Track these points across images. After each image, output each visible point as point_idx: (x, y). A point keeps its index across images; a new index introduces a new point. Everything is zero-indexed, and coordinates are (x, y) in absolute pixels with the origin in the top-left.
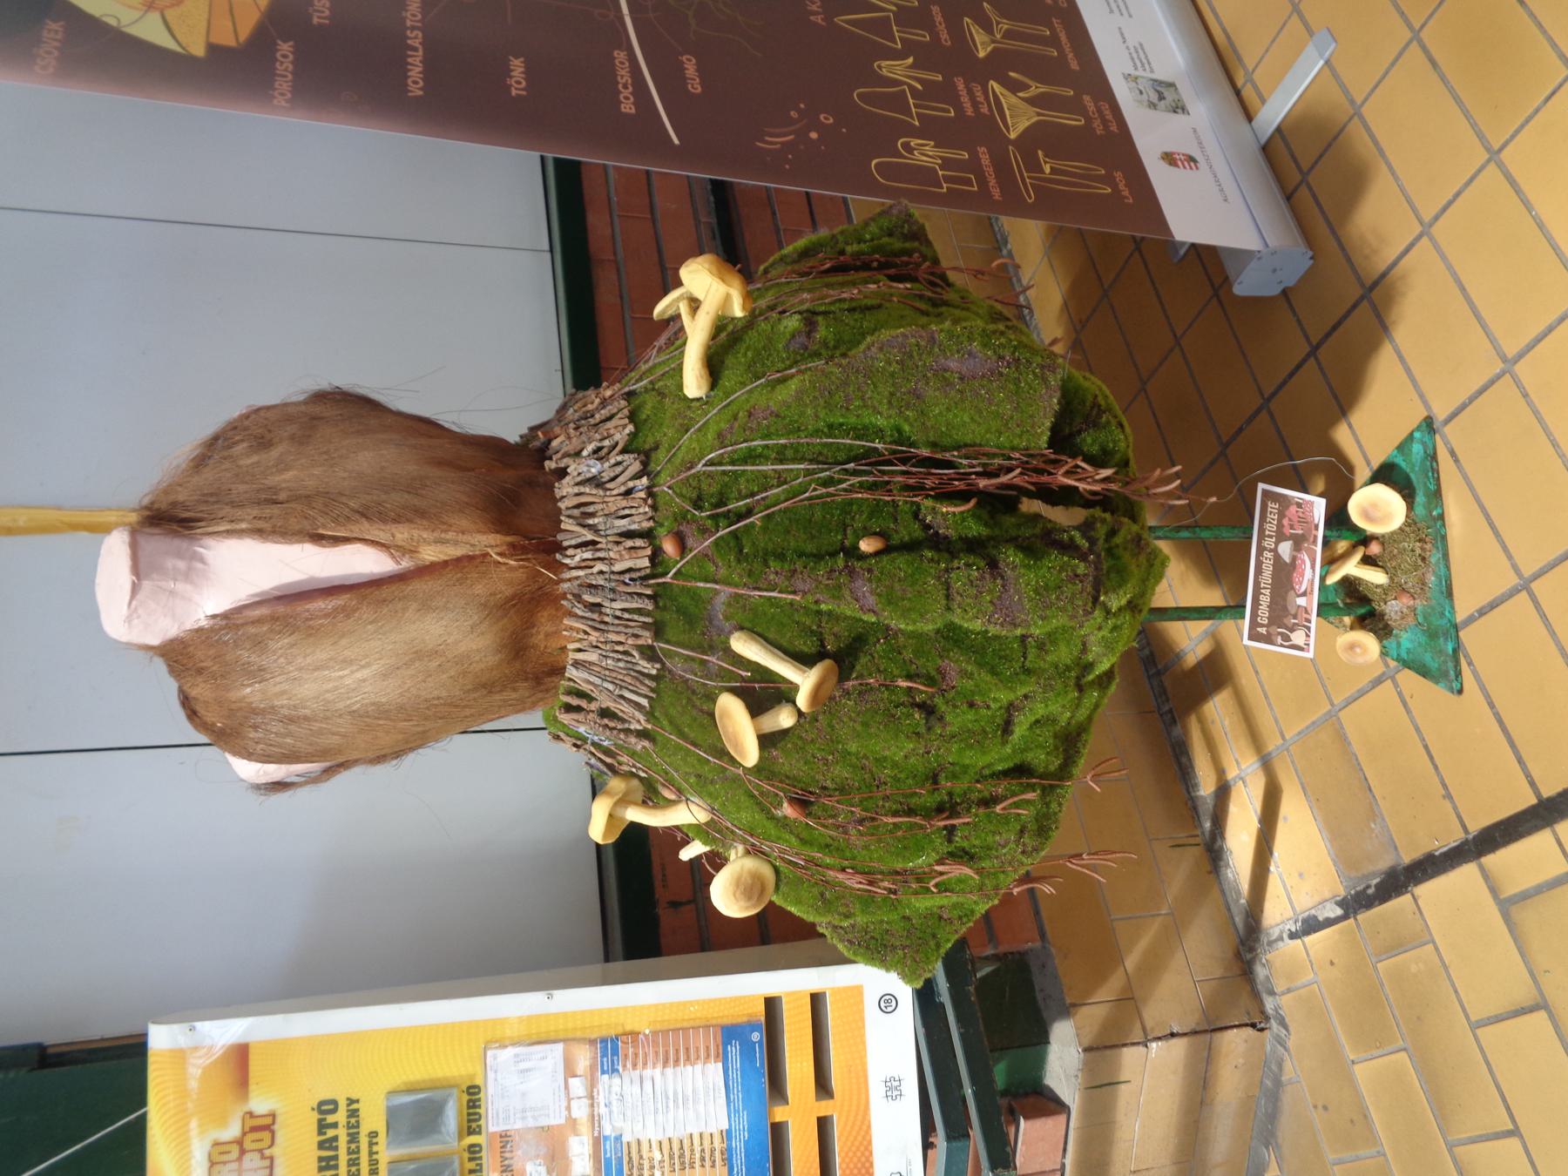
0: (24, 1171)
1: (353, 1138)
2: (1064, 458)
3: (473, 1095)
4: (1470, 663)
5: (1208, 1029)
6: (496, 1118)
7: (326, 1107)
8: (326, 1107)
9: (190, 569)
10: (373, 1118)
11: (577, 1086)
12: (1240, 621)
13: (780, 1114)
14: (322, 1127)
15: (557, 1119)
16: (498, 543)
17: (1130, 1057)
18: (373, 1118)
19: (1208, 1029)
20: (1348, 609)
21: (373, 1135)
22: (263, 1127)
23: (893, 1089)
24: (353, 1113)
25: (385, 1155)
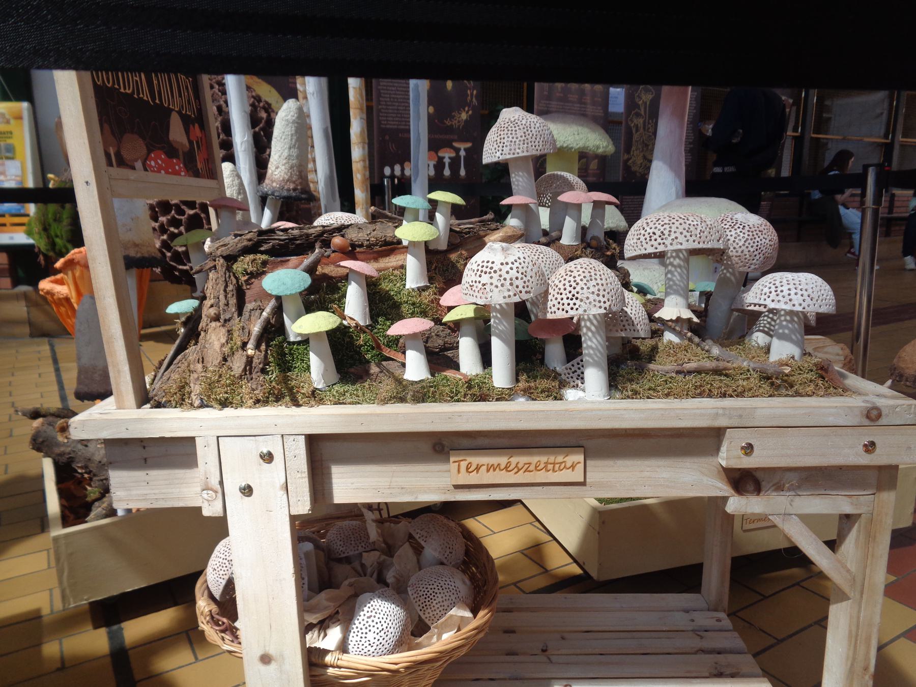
0: (3, 77)
1: (5, 137)
2: (404, 657)
3: (12, 158)
4: (543, 531)
5: (31, 323)
6: (9, 163)
7: (11, 133)
8: (11, 133)
9: (313, 182)
10: (9, 141)
11: (13, 177)
12: (841, 365)
13: (7, 216)
14: (7, 132)
15: (7, 173)
16: (97, 485)
17: (23, 303)
18: (9, 141)
19: (31, 323)
20: (103, 490)
21: (5, 141)
22: (8, 122)
23: (12, 238)
24: (10, 138)
25: (2, 143)
